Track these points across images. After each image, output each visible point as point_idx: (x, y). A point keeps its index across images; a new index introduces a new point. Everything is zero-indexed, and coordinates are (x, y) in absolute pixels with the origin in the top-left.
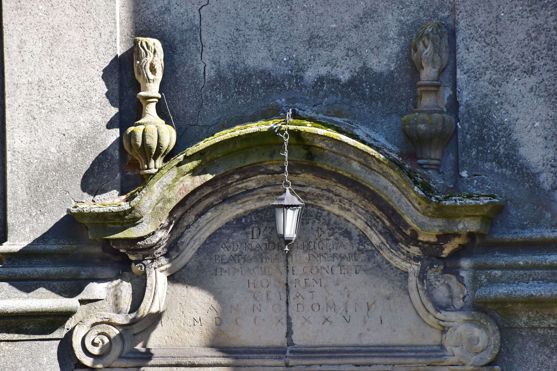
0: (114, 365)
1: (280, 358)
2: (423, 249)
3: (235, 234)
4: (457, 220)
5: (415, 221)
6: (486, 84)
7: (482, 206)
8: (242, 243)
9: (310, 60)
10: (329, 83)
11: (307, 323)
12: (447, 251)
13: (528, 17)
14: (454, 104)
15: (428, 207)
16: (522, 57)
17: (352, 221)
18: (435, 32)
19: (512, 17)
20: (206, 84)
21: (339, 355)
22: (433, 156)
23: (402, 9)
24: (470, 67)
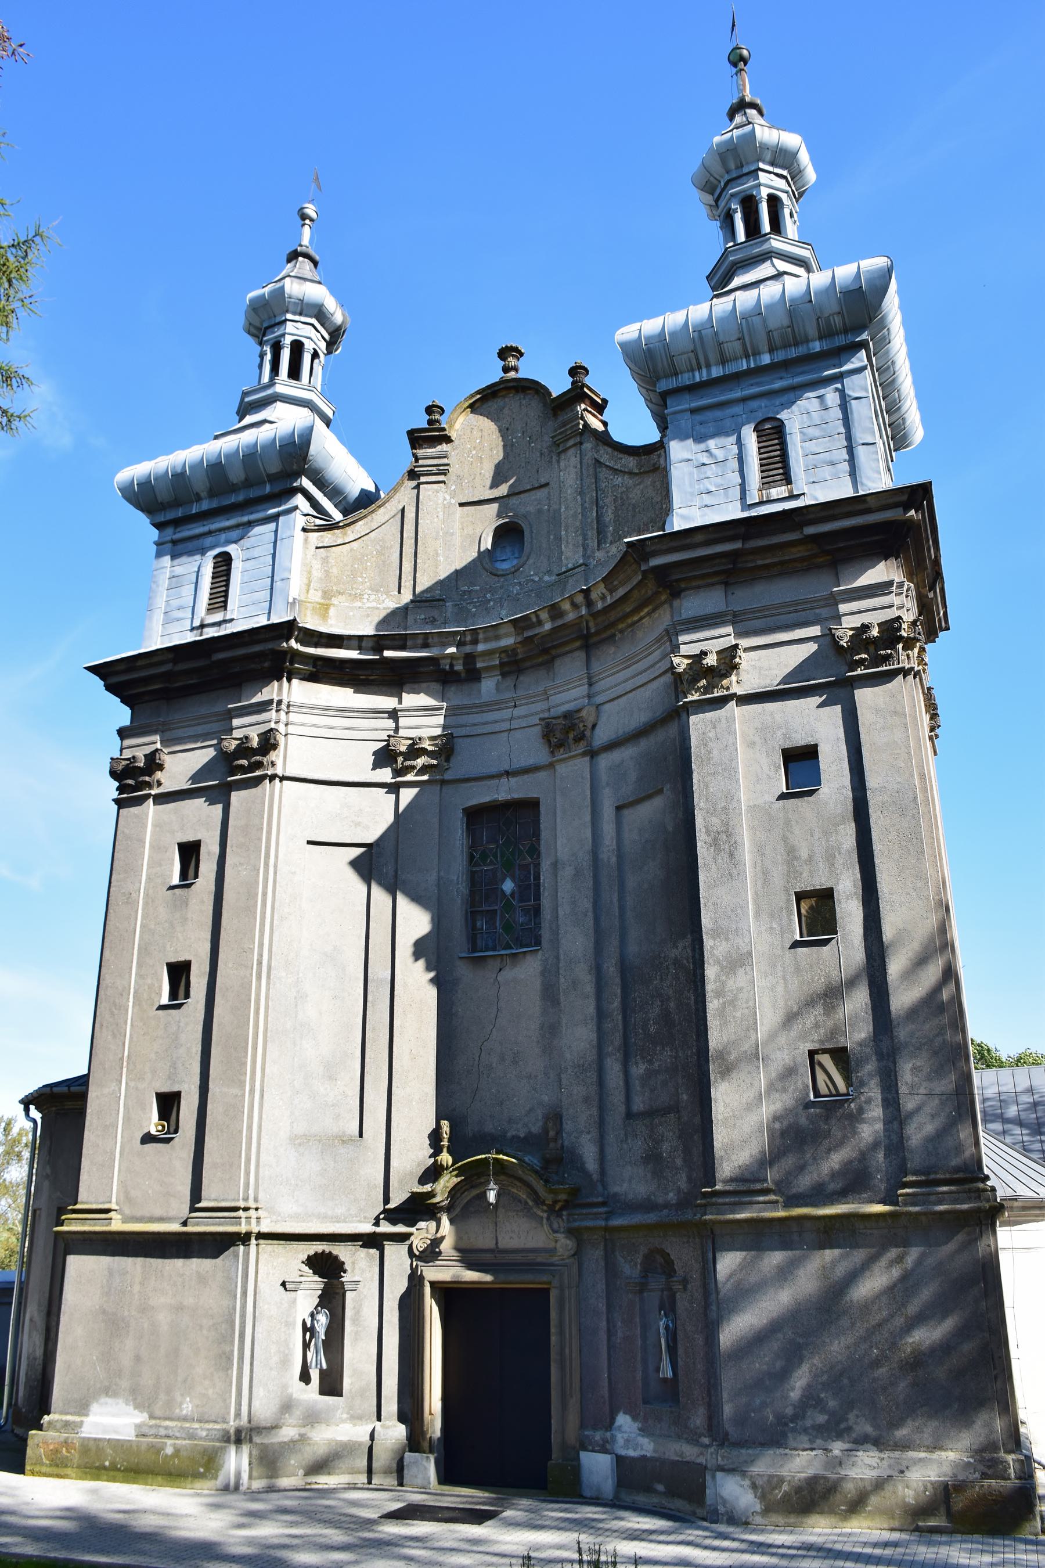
14: (562, 1146)
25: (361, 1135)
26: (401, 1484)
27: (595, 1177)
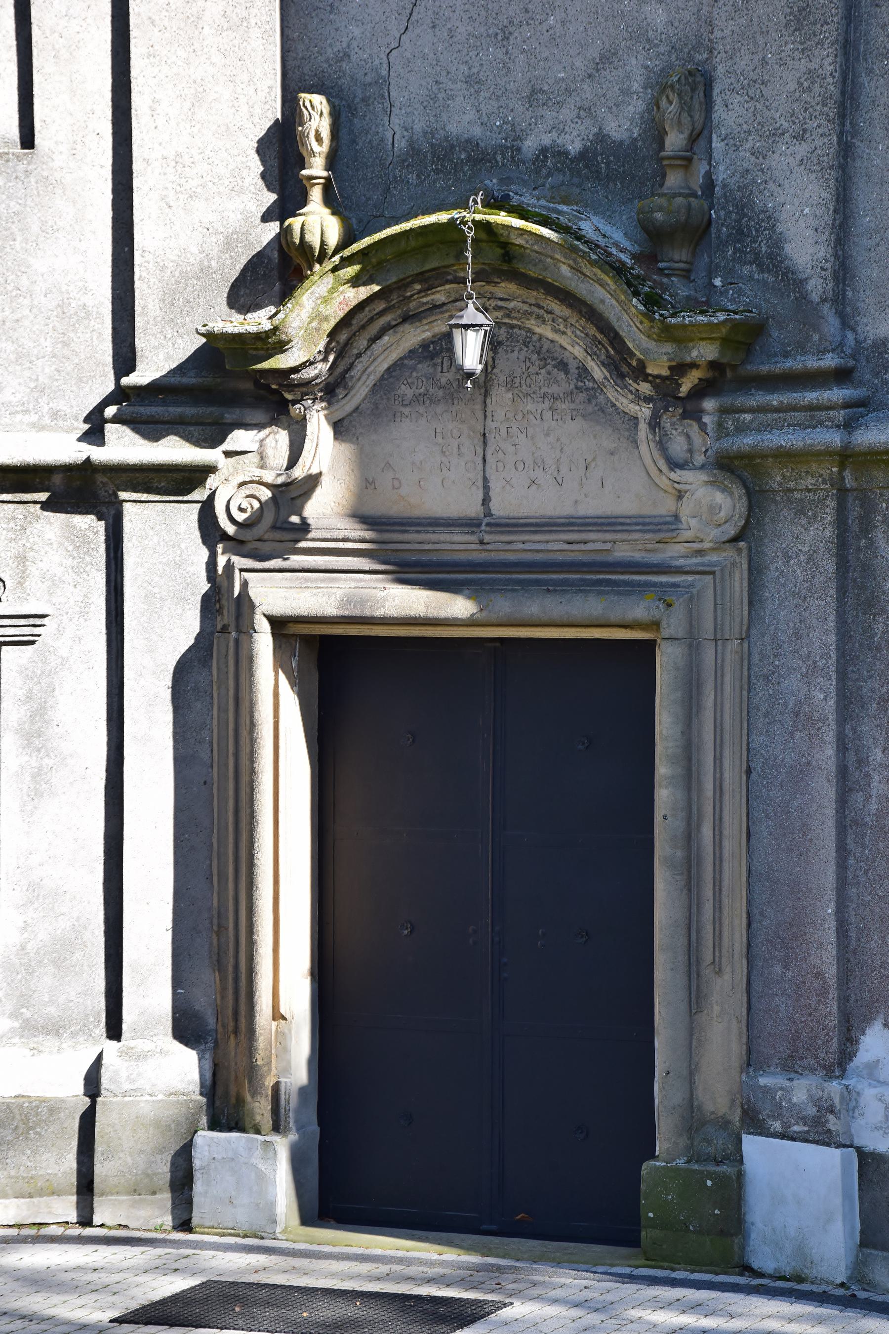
0: (266, 537)
1: (473, 533)
2: (655, 387)
3: (420, 366)
4: (691, 344)
5: (638, 347)
6: (748, 154)
7: (716, 324)
8: (428, 379)
9: (530, 125)
10: (554, 156)
11: (508, 487)
12: (685, 389)
13: (800, 59)
14: (709, 185)
15: (652, 327)
16: (791, 116)
17: (569, 348)
18: (683, 82)
19: (781, 59)
20: (395, 160)
21: (546, 529)
22: (677, 257)
23: (649, 50)
24: (729, 130)
25: (28, 140)
26: (184, 1225)
27: (816, 287)
